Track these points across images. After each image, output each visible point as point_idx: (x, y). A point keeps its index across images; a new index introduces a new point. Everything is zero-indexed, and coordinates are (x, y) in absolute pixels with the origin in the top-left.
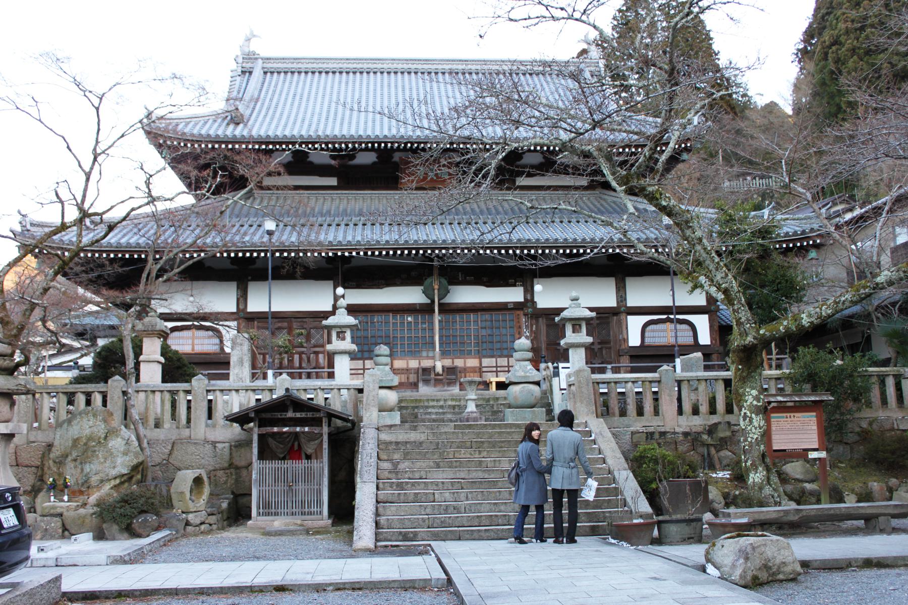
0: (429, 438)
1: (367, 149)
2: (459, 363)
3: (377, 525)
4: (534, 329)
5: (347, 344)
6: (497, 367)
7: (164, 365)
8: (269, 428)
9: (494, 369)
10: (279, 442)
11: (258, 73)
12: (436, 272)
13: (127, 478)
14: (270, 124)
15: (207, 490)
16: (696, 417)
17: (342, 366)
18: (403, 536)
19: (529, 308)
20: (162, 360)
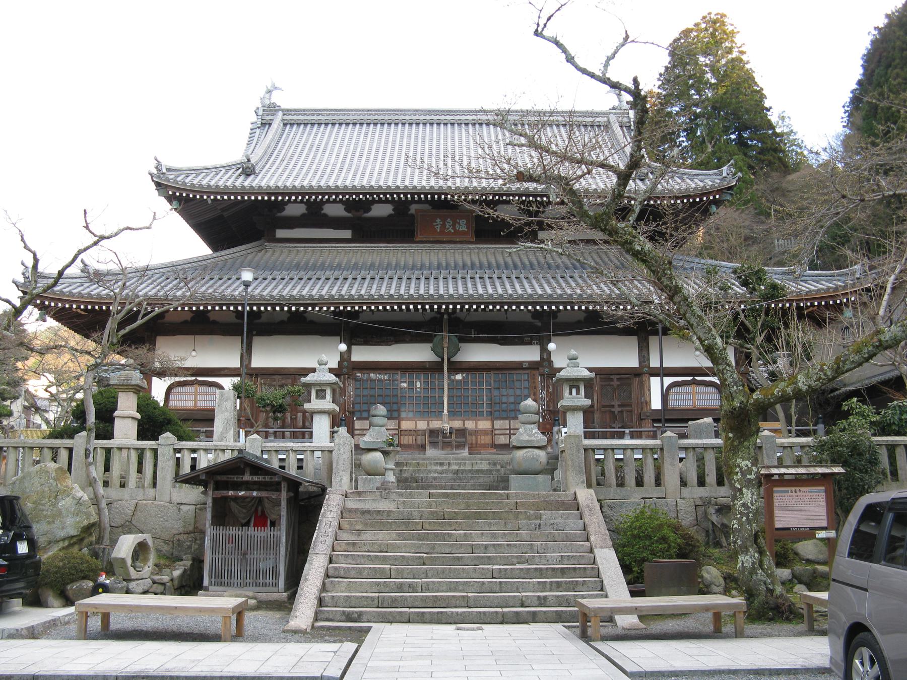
0: (400, 507)
1: (380, 201)
2: (470, 425)
3: (321, 602)
4: (550, 390)
5: (327, 404)
6: (510, 429)
7: (139, 421)
8: (224, 492)
9: (508, 432)
10: (242, 507)
11: (277, 124)
12: (445, 326)
13: (78, 540)
14: (281, 175)
15: (152, 558)
16: (701, 489)
17: (321, 426)
18: (346, 616)
19: (545, 367)
20: (138, 416)
